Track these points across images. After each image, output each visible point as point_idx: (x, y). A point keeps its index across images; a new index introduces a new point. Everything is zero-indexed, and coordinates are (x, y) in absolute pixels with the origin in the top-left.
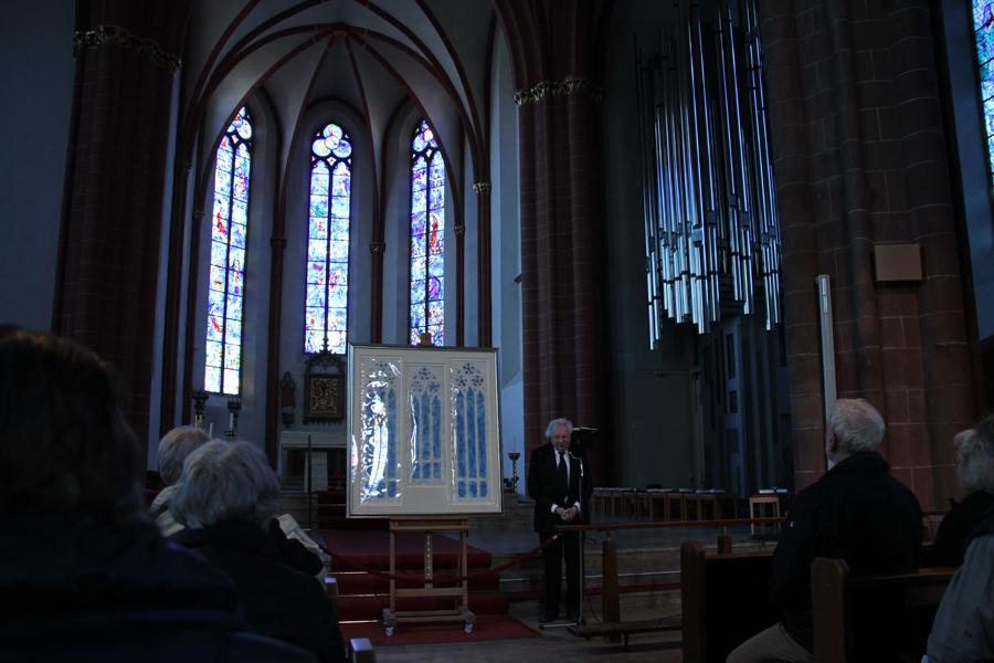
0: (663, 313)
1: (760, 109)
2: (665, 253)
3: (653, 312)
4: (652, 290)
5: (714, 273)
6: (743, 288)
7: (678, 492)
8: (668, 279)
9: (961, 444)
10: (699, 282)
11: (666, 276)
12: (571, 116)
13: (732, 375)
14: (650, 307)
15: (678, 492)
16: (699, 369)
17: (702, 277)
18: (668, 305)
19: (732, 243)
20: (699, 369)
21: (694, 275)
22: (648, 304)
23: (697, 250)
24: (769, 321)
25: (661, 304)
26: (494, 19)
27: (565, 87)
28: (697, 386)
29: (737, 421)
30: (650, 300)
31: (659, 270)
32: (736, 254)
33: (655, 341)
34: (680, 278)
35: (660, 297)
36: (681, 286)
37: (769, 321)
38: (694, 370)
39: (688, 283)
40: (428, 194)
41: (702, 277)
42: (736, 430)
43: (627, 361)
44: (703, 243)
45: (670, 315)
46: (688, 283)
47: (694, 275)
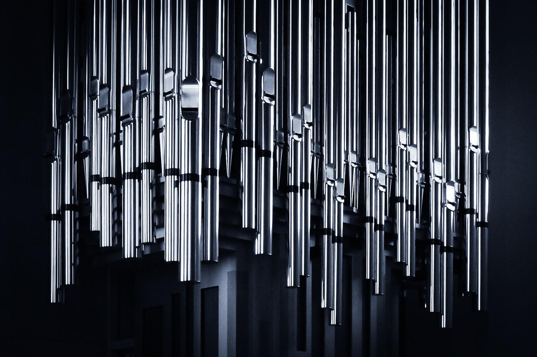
0: (85, 237)
2: (100, 130)
6: (257, 212)
8: (104, 175)
9: (232, 272)
10: (186, 185)
14: (54, 224)
17: (192, 177)
18: (100, 220)
19: (243, 123)
21: (175, 172)
22: (50, 217)
24: (291, 271)
26: (130, 101)
30: (54, 211)
31: (81, 155)
33: (62, 288)
34: (136, 175)
35: (82, 207)
37: (291, 271)
39: (158, 189)
40: (59, 222)
41: (192, 177)
44: (200, 116)
46: (158, 189)
47: (175, 172)
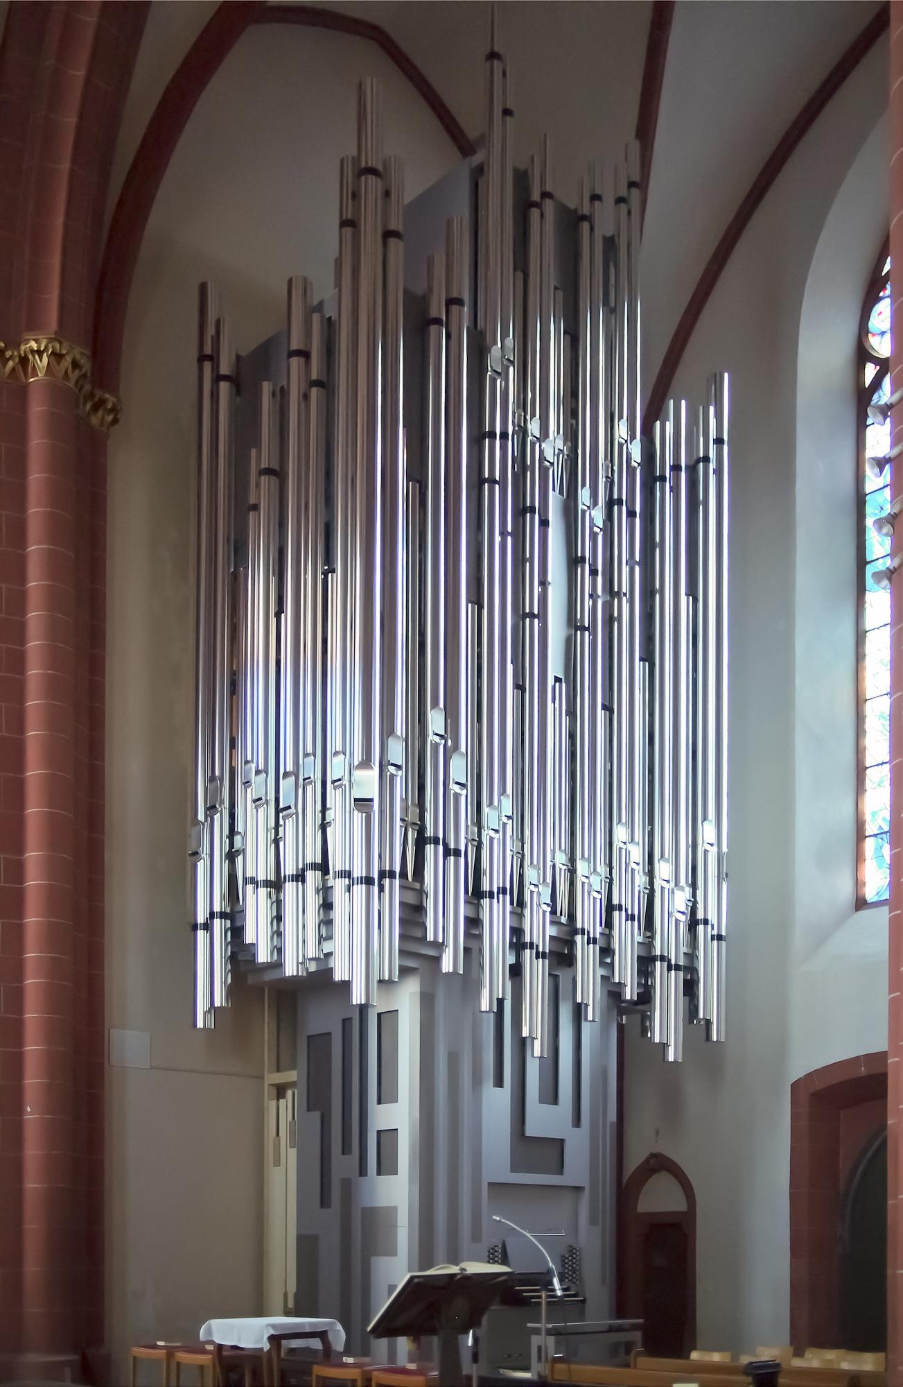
0: (240, 953)
1: (503, 534)
3: (209, 954)
4: (207, 897)
5: (392, 875)
7: (155, 1347)
11: (257, 863)
12: (36, 510)
13: (386, 1095)
15: (155, 1347)
16: (292, 1076)
18: (257, 931)
20: (292, 1076)
21: (347, 874)
22: (195, 927)
23: (358, 817)
25: (237, 932)
27: (24, 361)
28: (283, 1114)
29: (396, 1192)
32: (436, 841)
34: (300, 877)
35: (234, 916)
36: (300, 901)
38: (279, 1078)
42: (393, 1210)
43: (131, 1044)
45: (263, 956)
